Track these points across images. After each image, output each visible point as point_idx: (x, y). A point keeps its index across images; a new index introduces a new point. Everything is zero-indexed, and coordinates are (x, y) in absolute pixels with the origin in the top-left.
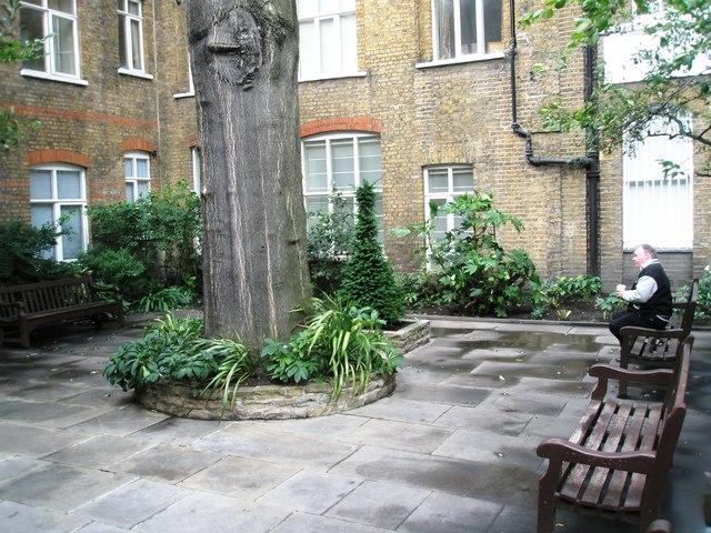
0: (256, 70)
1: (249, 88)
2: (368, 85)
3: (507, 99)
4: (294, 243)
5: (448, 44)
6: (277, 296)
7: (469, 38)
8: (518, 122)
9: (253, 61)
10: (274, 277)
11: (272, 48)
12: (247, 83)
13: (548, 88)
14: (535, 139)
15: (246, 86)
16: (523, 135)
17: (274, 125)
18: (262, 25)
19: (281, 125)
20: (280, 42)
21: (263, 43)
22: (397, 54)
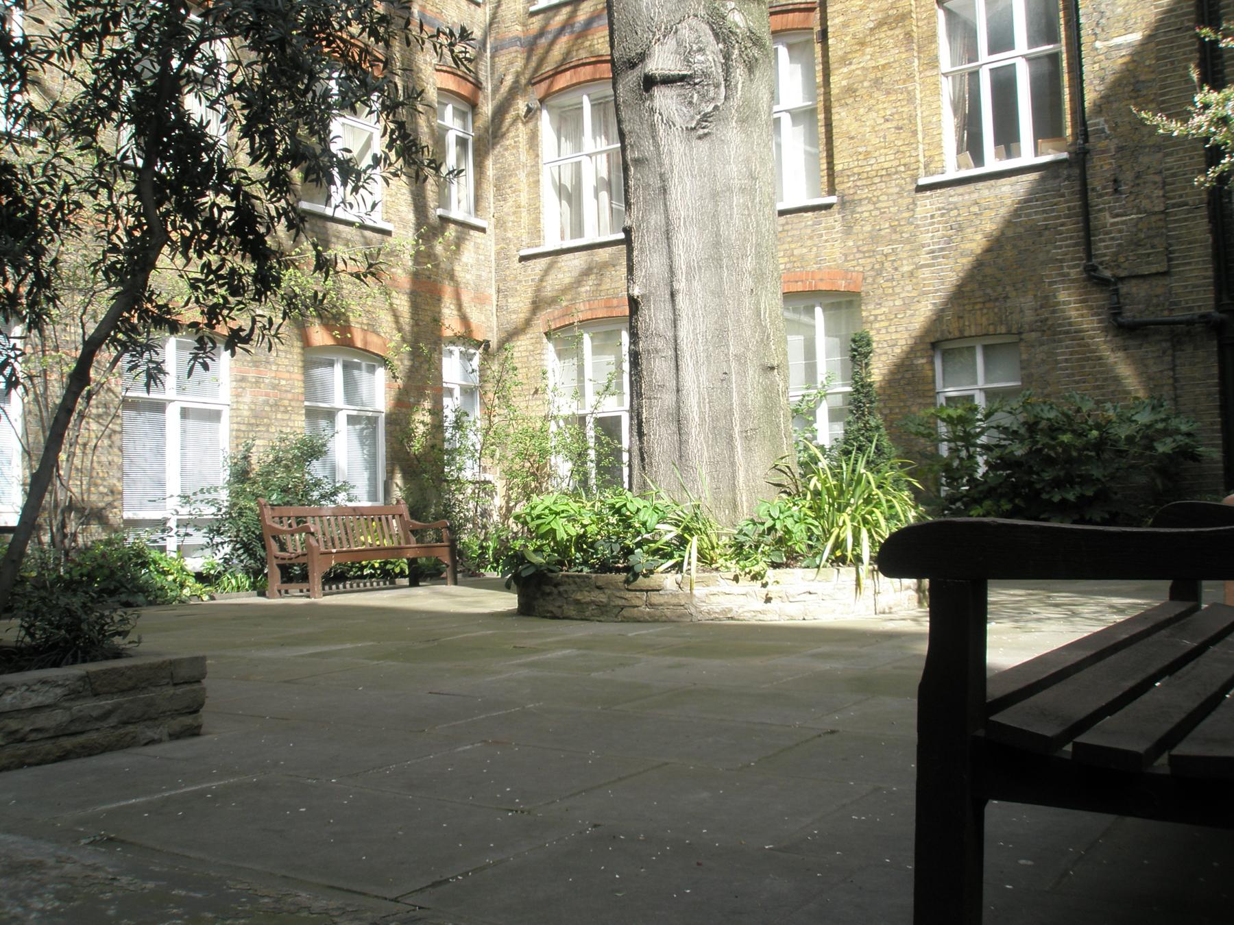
0: (716, 108)
1: (706, 135)
2: (838, 216)
3: (1071, 227)
4: (772, 368)
5: (972, 145)
6: (748, 450)
7: (1007, 136)
8: (1094, 261)
9: (711, 94)
10: (743, 419)
11: (739, 74)
12: (701, 128)
13: (1145, 203)
14: (1124, 288)
15: (701, 132)
16: (1103, 283)
17: (742, 190)
18: (724, 41)
19: (753, 189)
20: (751, 67)
21: (727, 69)
22: (886, 165)
